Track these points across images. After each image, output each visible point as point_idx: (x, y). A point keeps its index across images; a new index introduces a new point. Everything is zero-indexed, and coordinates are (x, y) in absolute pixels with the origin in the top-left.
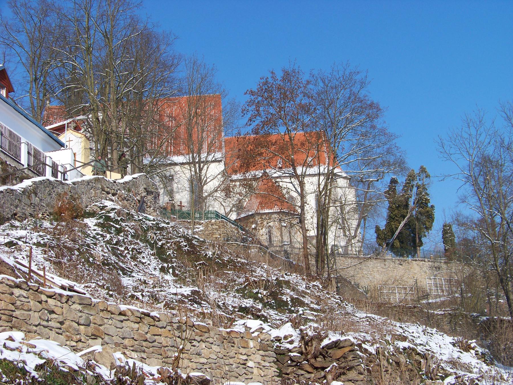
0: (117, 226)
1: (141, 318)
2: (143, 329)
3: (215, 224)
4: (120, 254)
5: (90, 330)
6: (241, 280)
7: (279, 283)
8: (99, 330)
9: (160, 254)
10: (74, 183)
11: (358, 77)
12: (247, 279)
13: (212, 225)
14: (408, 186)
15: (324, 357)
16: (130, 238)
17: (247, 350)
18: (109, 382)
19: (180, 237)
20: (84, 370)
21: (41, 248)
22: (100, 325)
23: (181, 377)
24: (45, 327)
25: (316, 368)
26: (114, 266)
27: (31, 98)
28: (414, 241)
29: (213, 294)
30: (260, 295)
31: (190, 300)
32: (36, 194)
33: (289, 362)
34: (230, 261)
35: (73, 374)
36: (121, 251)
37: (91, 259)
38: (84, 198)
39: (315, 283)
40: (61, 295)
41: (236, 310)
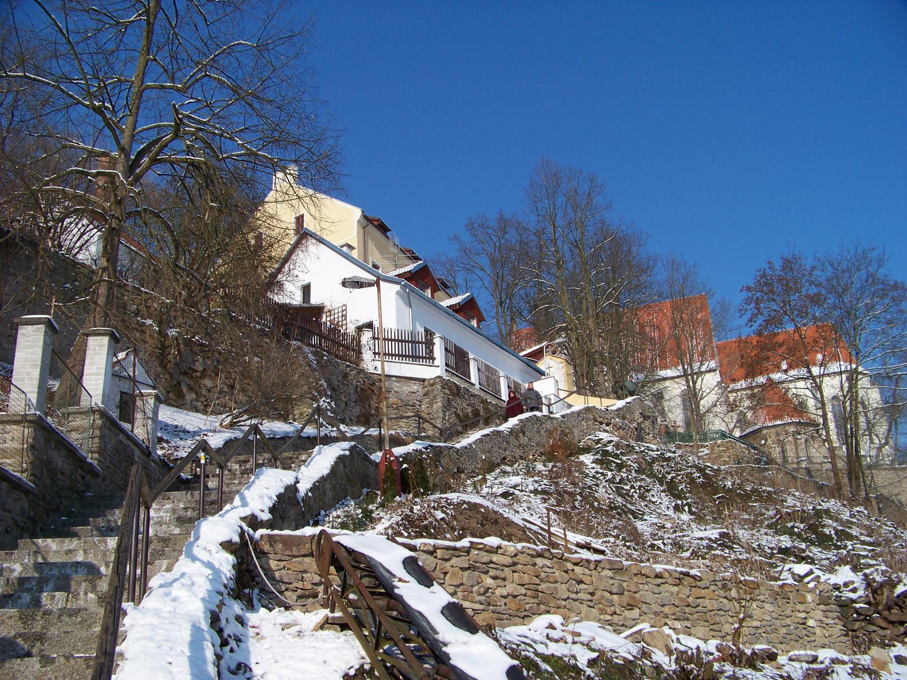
0: (617, 461)
1: (679, 579)
2: (684, 592)
4: (627, 494)
5: (625, 599)
6: (771, 513)
7: (818, 514)
8: (634, 598)
9: (672, 489)
10: (563, 416)
11: (873, 255)
12: (778, 512)
13: (718, 446)
15: (901, 608)
16: (634, 475)
17: (805, 605)
18: (671, 673)
19: (691, 467)
20: (640, 659)
21: (540, 496)
22: (636, 593)
23: (745, 654)
24: (574, 600)
25: (892, 623)
26: (622, 509)
27: (498, 323)
29: (743, 534)
30: (796, 530)
31: (720, 545)
32: (524, 434)
33: (855, 615)
34: (753, 491)
35: (629, 666)
36: (626, 490)
37: (596, 504)
38: (576, 432)
39: (858, 509)
40: (588, 561)
41: (775, 552)
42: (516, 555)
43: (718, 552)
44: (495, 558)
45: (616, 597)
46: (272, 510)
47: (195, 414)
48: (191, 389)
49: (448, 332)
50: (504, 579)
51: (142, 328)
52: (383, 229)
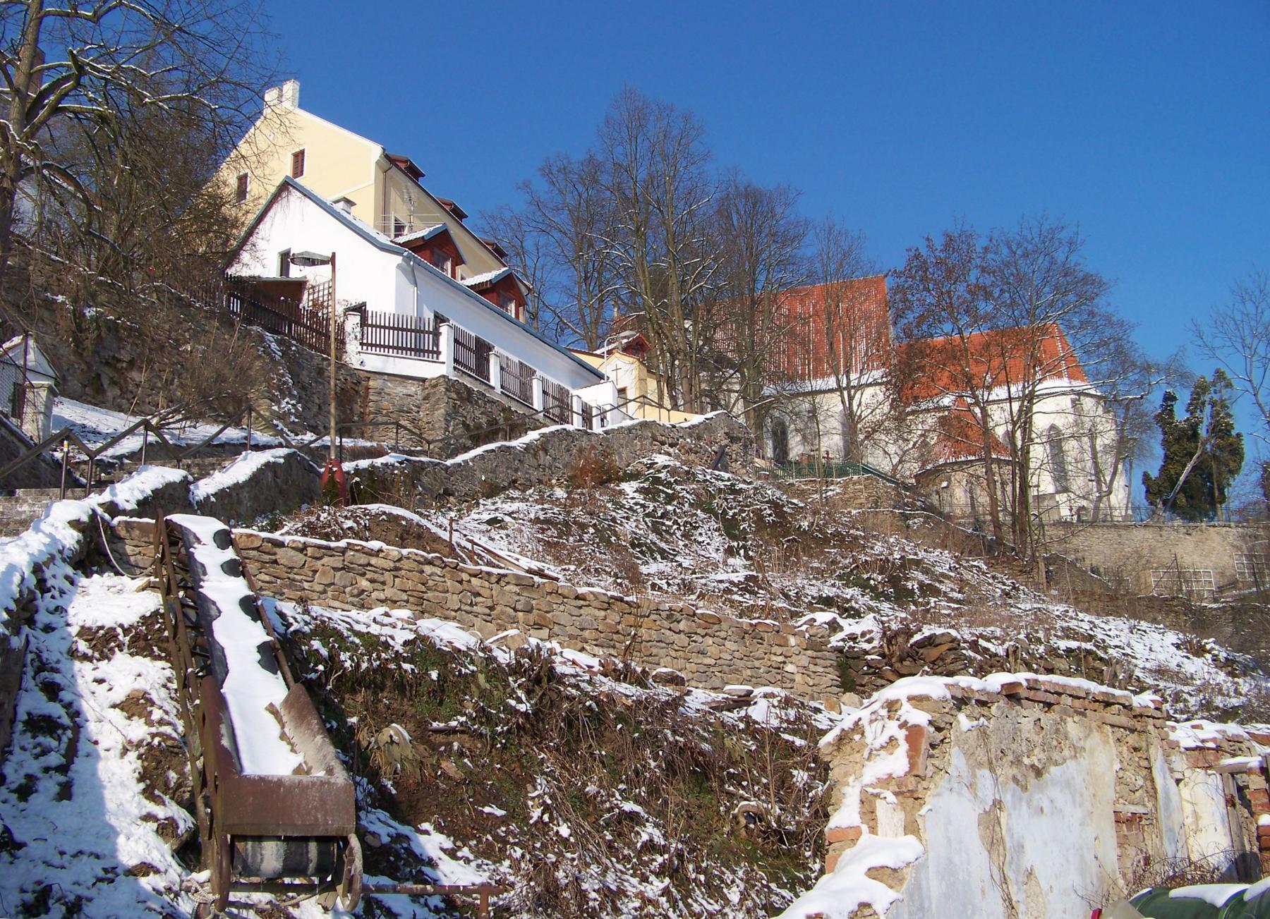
3: (859, 482)
5: (532, 617)
7: (905, 564)
8: (545, 618)
9: (730, 528)
11: (1064, 235)
12: (855, 561)
13: (854, 484)
14: (1195, 404)
24: (467, 612)
28: (1211, 494)
30: (872, 582)
32: (546, 452)
40: (489, 574)
42: (399, 560)
43: (736, 597)
44: (373, 561)
45: (520, 614)
46: (139, 503)
47: (116, 414)
48: (114, 382)
49: (478, 321)
50: (384, 583)
51: (50, 305)
52: (413, 173)
